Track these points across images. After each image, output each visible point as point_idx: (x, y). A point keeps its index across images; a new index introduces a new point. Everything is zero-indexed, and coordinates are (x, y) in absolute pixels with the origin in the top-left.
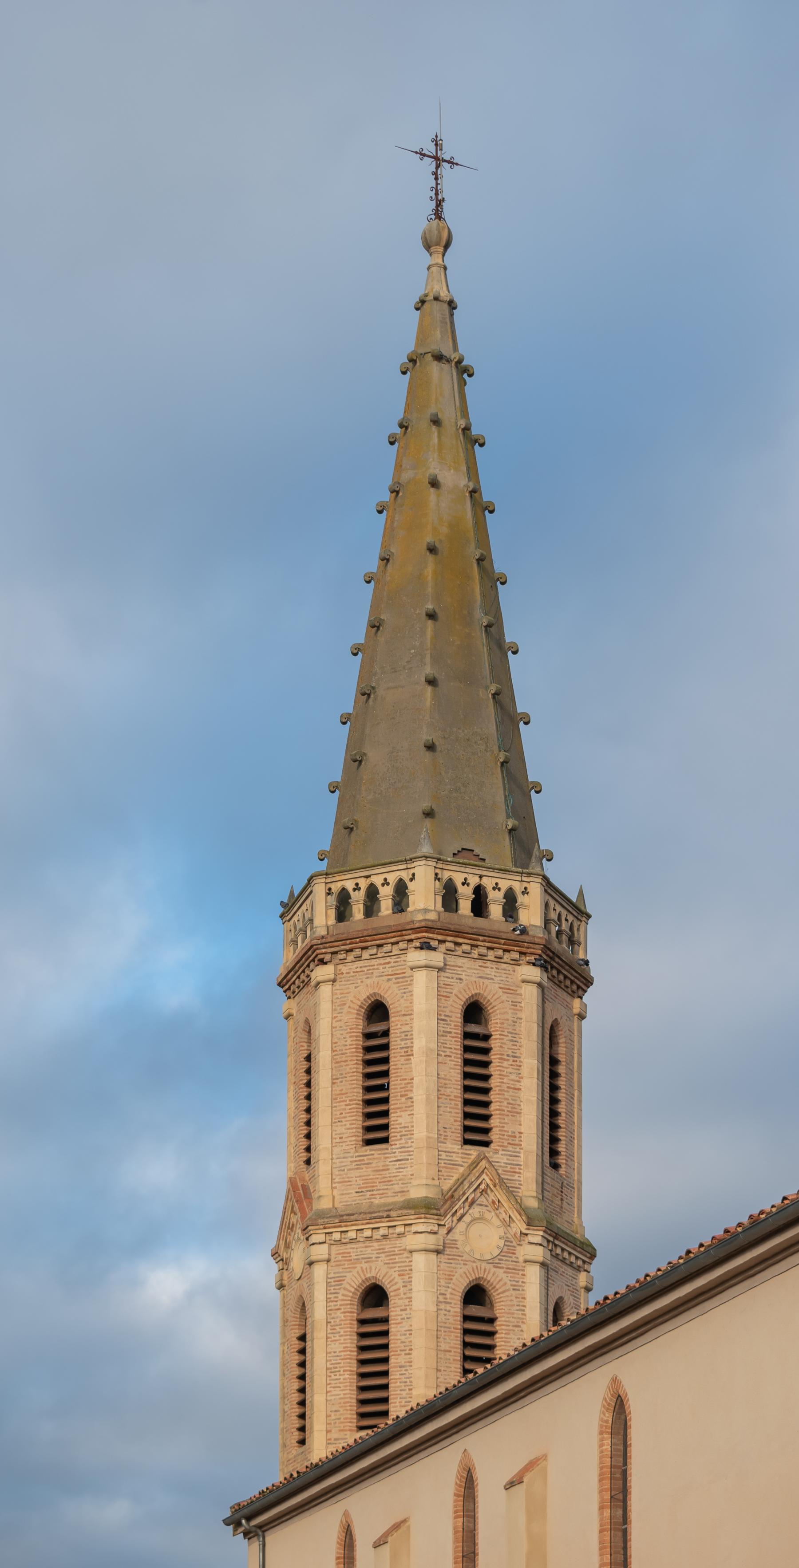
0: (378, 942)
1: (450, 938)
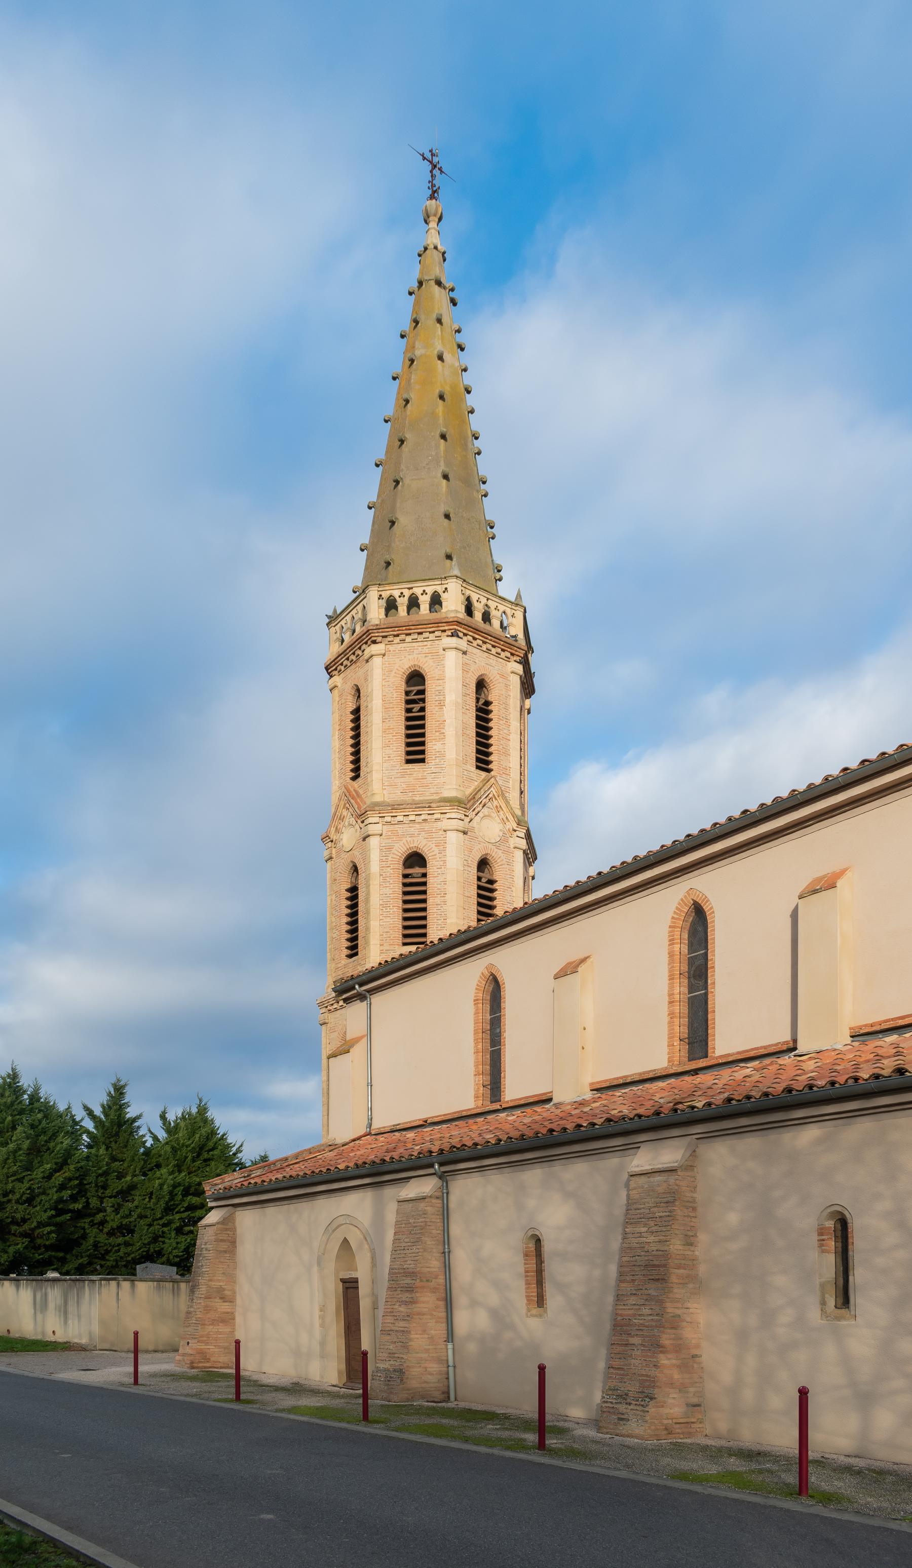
0: (419, 631)
1: (470, 633)
